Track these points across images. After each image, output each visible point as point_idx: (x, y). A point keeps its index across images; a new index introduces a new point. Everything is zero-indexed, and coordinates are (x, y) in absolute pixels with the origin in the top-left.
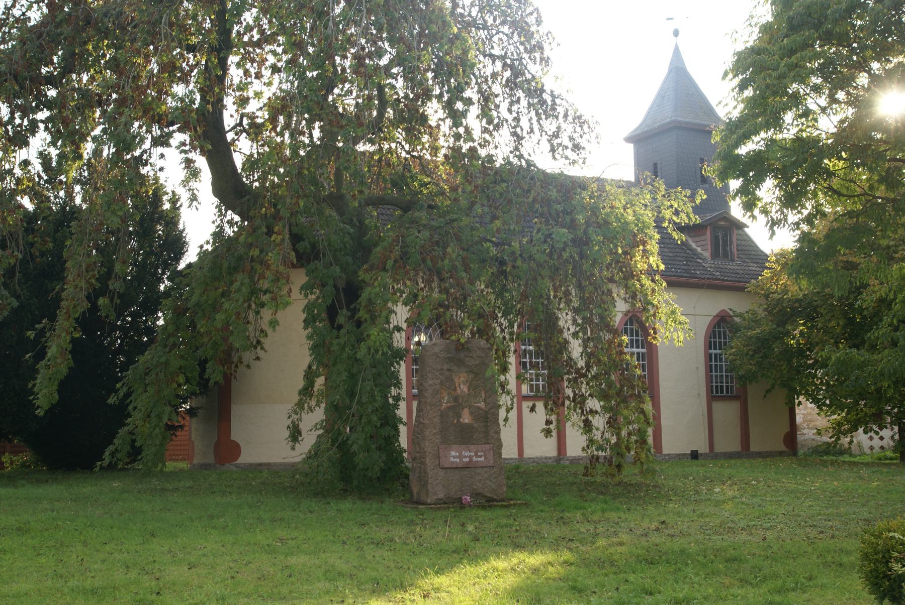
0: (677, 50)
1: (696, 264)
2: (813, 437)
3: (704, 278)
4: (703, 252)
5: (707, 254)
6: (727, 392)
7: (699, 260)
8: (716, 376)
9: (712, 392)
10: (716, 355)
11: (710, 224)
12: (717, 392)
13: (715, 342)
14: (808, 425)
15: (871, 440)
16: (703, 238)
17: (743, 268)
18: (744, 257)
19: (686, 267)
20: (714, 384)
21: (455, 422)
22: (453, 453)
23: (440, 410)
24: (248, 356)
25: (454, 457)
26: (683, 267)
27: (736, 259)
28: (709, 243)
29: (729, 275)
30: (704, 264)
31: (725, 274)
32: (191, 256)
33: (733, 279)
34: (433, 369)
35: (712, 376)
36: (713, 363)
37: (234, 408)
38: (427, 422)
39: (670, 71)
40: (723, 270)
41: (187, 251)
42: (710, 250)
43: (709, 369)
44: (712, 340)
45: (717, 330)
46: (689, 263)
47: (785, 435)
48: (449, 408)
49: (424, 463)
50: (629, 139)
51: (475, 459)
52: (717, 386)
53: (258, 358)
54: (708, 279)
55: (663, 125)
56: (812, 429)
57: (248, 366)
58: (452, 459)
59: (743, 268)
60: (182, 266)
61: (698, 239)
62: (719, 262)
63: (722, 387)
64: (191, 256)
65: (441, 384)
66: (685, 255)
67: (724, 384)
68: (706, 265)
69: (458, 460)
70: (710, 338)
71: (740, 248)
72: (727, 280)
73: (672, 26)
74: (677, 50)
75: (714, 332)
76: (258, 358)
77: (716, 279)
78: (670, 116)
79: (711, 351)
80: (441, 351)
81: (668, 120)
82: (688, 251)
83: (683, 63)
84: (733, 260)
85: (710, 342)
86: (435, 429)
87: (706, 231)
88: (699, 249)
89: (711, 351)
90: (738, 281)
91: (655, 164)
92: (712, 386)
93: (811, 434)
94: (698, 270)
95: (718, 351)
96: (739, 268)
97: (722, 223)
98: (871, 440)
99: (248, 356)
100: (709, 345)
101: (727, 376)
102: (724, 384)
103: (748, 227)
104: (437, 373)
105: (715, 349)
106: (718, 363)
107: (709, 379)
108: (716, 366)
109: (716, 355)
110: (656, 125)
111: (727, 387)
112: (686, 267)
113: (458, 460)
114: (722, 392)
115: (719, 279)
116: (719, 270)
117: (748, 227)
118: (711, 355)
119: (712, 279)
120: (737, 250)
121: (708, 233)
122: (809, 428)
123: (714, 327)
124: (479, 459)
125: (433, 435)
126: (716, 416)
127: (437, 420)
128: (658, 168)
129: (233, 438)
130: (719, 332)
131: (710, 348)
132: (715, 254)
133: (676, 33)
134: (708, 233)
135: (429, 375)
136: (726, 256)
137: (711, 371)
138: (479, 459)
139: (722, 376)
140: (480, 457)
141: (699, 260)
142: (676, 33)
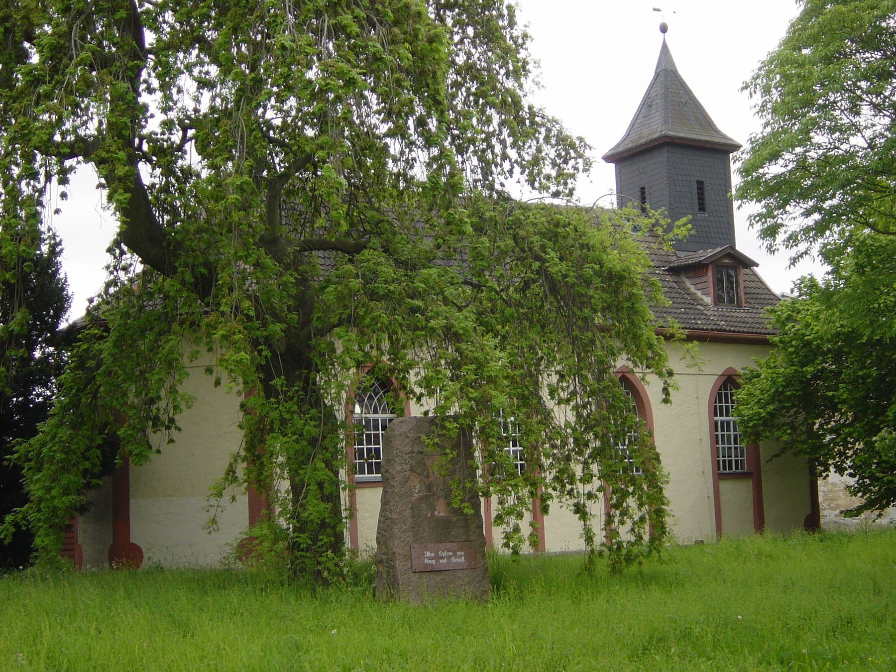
0: (665, 48)
1: (696, 312)
2: (836, 519)
3: (707, 329)
4: (704, 297)
5: (708, 300)
6: (737, 468)
7: (699, 307)
8: (723, 448)
9: (719, 470)
10: (722, 423)
11: (711, 263)
12: (725, 469)
13: (721, 407)
14: (829, 505)
15: (211, 373)
16: (704, 279)
17: (753, 315)
18: (753, 301)
19: (684, 316)
20: (721, 459)
21: (429, 515)
22: (428, 554)
23: (410, 501)
24: (157, 438)
25: (429, 558)
26: (681, 316)
27: (744, 304)
28: (711, 285)
29: (736, 324)
30: (705, 312)
31: (732, 324)
32: (76, 313)
33: (741, 330)
34: (401, 452)
35: (718, 448)
36: (720, 433)
37: (132, 501)
38: (395, 516)
39: (657, 75)
40: (728, 319)
41: (70, 306)
42: (712, 294)
43: (715, 440)
44: (718, 405)
45: (723, 392)
46: (688, 310)
47: (806, 519)
48: (421, 498)
49: (393, 567)
50: (608, 159)
51: (453, 560)
52: (724, 461)
53: (171, 441)
54: (712, 330)
55: (652, 141)
56: (833, 509)
57: (158, 452)
58: (426, 561)
59: (753, 315)
60: (63, 325)
61: (696, 281)
62: (724, 309)
63: (730, 462)
64: (76, 313)
65: (412, 470)
66: (683, 301)
67: (733, 459)
68: (709, 313)
69: (434, 562)
70: (716, 403)
71: (748, 290)
72: (734, 331)
73: (659, 19)
74: (665, 48)
75: (720, 395)
76: (171, 441)
77: (721, 330)
78: (659, 129)
79: (716, 418)
80: (411, 430)
81: (657, 135)
82: (686, 296)
83: (675, 66)
84: (739, 306)
85: (716, 407)
86: (405, 524)
87: (707, 270)
88: (699, 293)
89: (716, 418)
90: (747, 332)
91: (643, 189)
92: (719, 461)
93: (833, 516)
94: (699, 319)
95: (724, 418)
96: (748, 315)
97: (727, 261)
98: (211, 373)
99: (157, 438)
100: (715, 411)
101: (736, 448)
102: (733, 459)
103: (757, 265)
104: (406, 457)
105: (721, 415)
106: (725, 433)
107: (715, 452)
108: (723, 436)
109: (722, 423)
110: (643, 141)
111: (736, 461)
112: (684, 316)
113: (434, 562)
114: (730, 468)
115: (725, 331)
116: (724, 318)
117: (757, 265)
118: (716, 423)
119: (717, 330)
120: (745, 294)
121: (710, 273)
122: (831, 508)
123: (720, 389)
124: (459, 560)
125: (403, 532)
126: (723, 498)
127: (408, 513)
128: (647, 193)
129: (132, 541)
130: (726, 395)
131: (716, 415)
132: (718, 300)
133: (664, 29)
134: (710, 273)
135: (397, 459)
136: (731, 301)
137: (717, 443)
138: (459, 560)
139: (730, 448)
140: (461, 556)
141: (699, 307)
142: (664, 29)
